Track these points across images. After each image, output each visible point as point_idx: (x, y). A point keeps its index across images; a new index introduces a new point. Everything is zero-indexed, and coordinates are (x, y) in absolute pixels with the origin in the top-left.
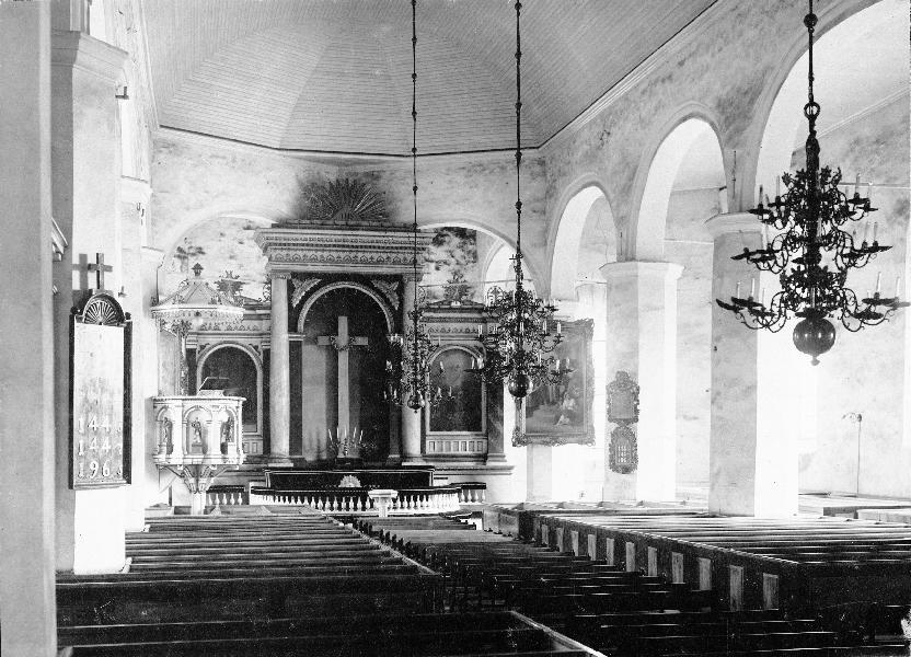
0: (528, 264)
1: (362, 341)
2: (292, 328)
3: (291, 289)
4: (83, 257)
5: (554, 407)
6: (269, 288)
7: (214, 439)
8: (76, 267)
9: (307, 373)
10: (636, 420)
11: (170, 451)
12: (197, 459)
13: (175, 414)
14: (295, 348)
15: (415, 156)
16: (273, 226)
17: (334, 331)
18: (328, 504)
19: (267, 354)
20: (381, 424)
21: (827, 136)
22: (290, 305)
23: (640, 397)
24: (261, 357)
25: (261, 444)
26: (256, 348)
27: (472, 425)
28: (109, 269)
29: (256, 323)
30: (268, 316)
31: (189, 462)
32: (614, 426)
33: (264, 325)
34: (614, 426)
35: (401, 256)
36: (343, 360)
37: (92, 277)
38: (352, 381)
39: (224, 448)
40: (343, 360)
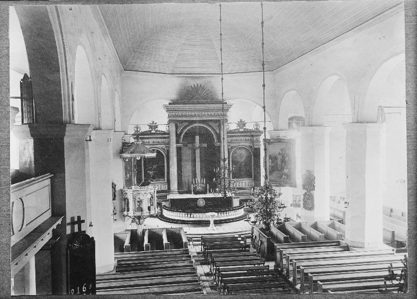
0: (268, 114)
1: (206, 145)
2: (177, 142)
3: (177, 127)
4: (72, 218)
5: (280, 172)
6: (169, 127)
7: (145, 206)
8: (69, 224)
9: (184, 158)
10: (314, 189)
11: (128, 210)
12: (138, 214)
13: (130, 197)
14: (179, 150)
15: (222, 74)
16: (170, 104)
17: (193, 142)
18: (189, 215)
19: (168, 152)
20: (212, 178)
21: (397, 54)
22: (176, 132)
23: (315, 180)
24: (166, 153)
25: (166, 185)
26: (164, 149)
27: (249, 176)
28: (83, 221)
29: (164, 140)
30: (168, 137)
31: (136, 215)
32: (305, 191)
33: (167, 140)
34: (305, 191)
35: (219, 113)
36: (198, 152)
37: (76, 226)
38: (201, 161)
39: (149, 208)
40: (198, 152)
